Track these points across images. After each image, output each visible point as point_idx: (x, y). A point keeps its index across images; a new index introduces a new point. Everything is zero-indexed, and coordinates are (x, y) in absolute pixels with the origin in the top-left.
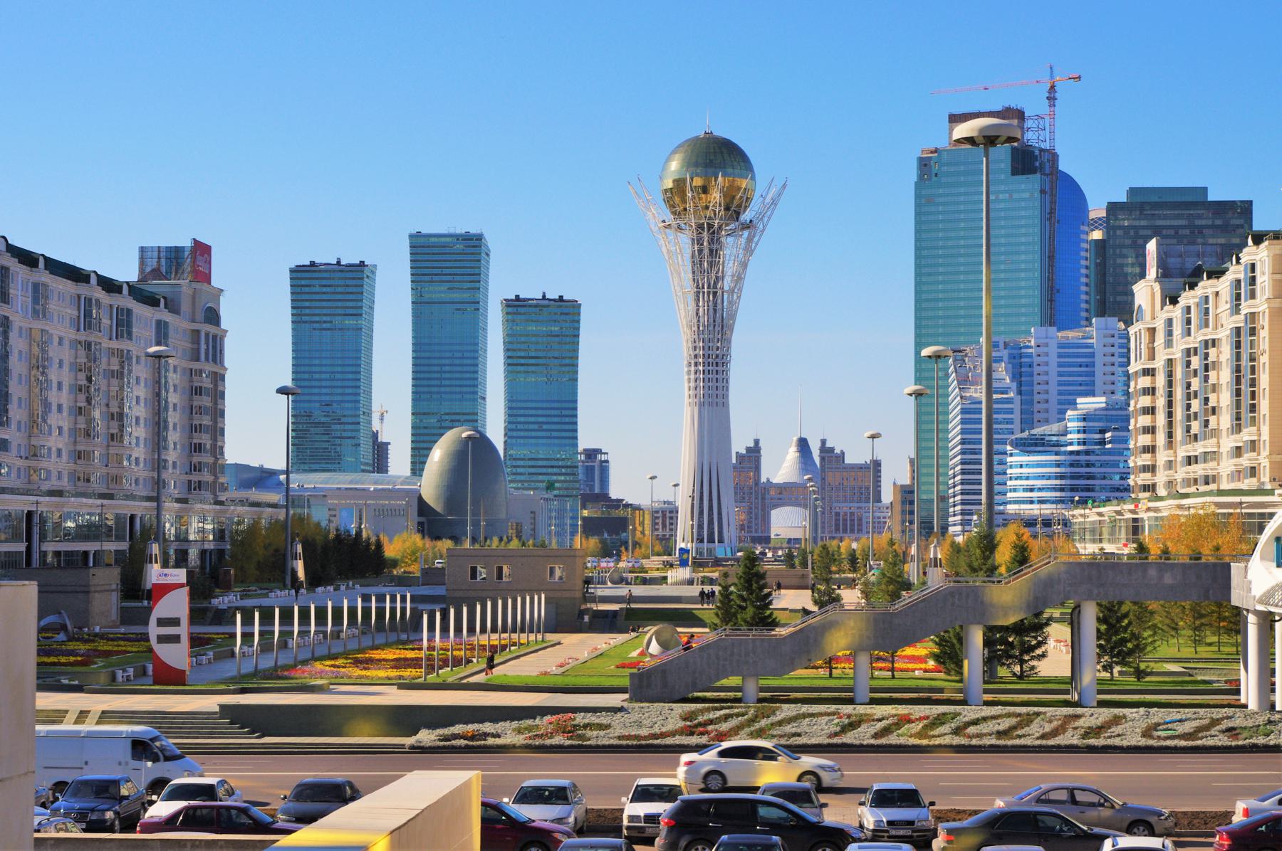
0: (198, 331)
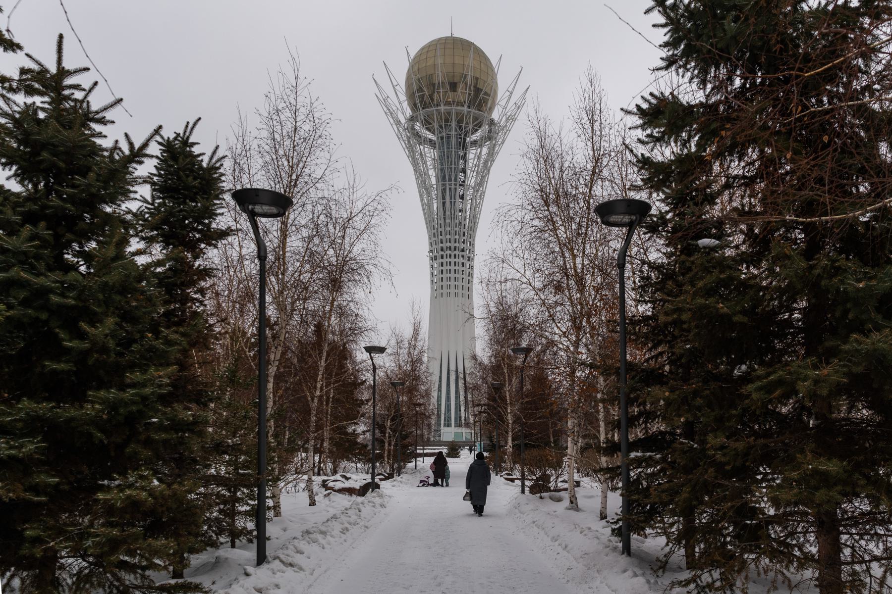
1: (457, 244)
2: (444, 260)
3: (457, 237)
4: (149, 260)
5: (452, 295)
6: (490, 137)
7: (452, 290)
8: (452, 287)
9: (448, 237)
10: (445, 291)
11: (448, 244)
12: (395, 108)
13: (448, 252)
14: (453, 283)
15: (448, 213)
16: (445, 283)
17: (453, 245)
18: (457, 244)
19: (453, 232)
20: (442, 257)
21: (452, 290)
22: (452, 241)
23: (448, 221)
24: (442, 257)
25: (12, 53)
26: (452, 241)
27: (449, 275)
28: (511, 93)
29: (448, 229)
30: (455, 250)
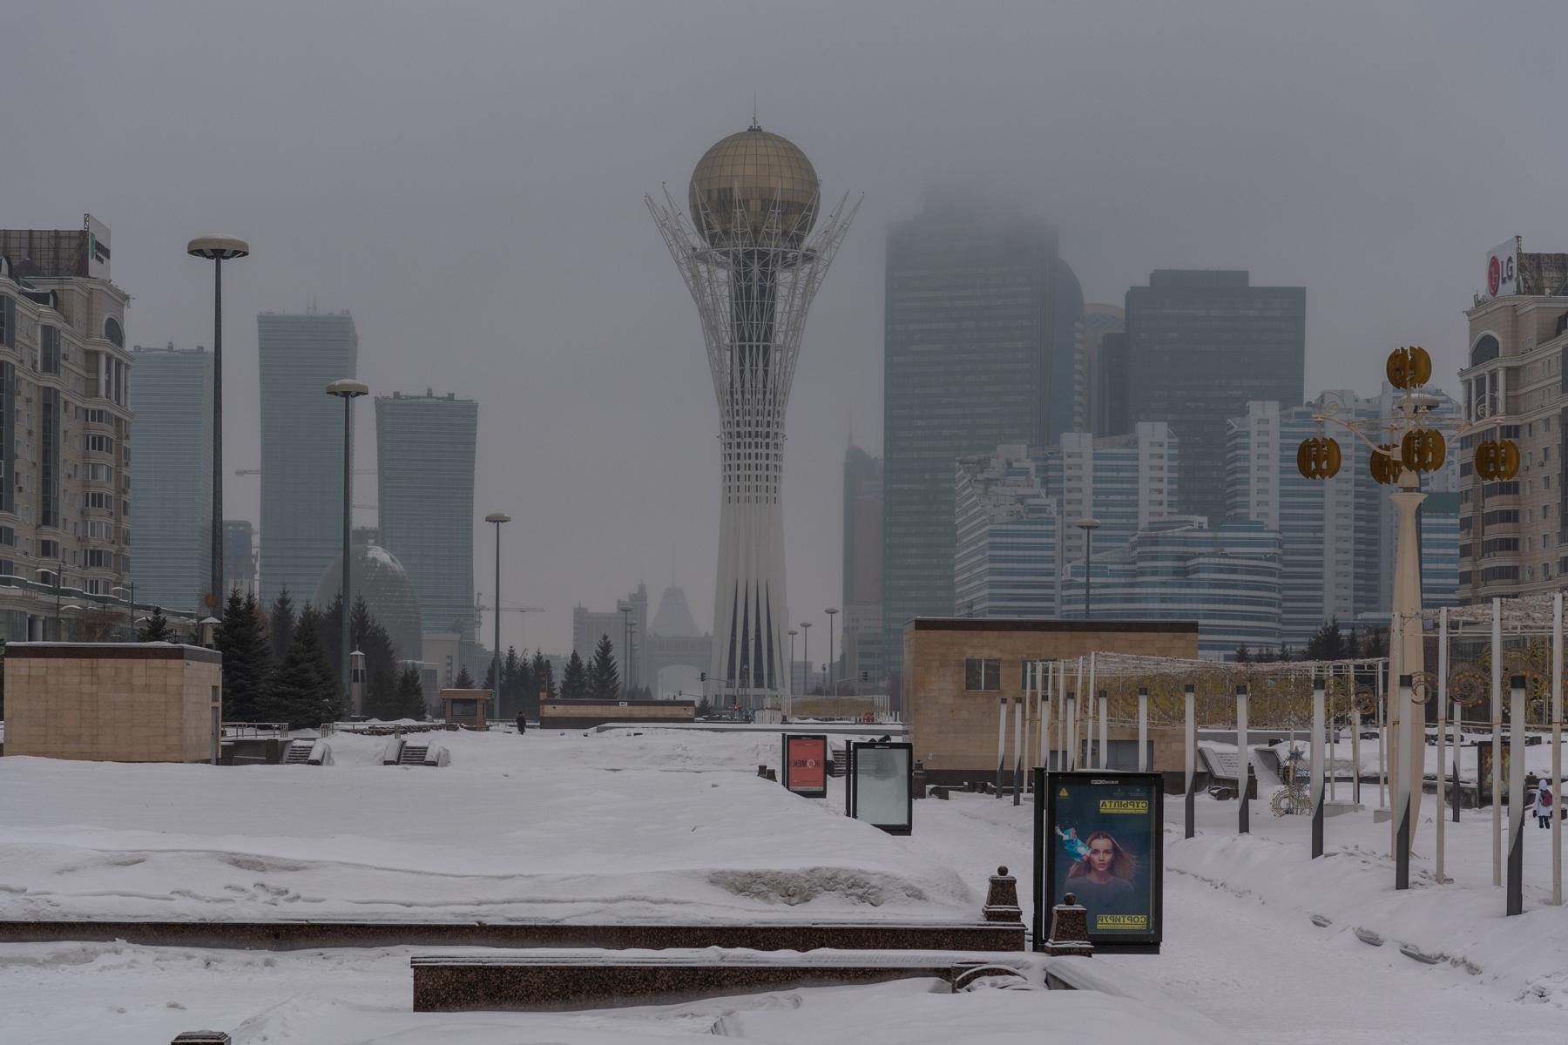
0: (97, 354)
8: (753, 489)
11: (748, 429)
13: (748, 440)
15: (747, 385)
17: (753, 429)
19: (754, 412)
23: (747, 396)
29: (747, 407)
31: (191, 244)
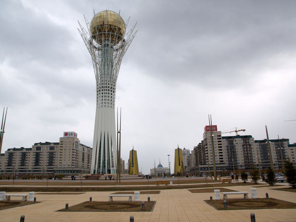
1: (109, 85)
2: (104, 92)
3: (109, 82)
4: (223, 192)
5: (103, 106)
6: (122, 47)
7: (107, 105)
9: (106, 82)
10: (104, 104)
11: (106, 85)
12: (85, 32)
13: (106, 88)
14: (107, 101)
16: (104, 98)
17: (107, 86)
18: (109, 85)
20: (103, 91)
21: (107, 105)
22: (107, 84)
24: (103, 91)
25: (152, 168)
26: (107, 84)
27: (105, 98)
28: (132, 31)
30: (108, 87)
31: (136, 151)
